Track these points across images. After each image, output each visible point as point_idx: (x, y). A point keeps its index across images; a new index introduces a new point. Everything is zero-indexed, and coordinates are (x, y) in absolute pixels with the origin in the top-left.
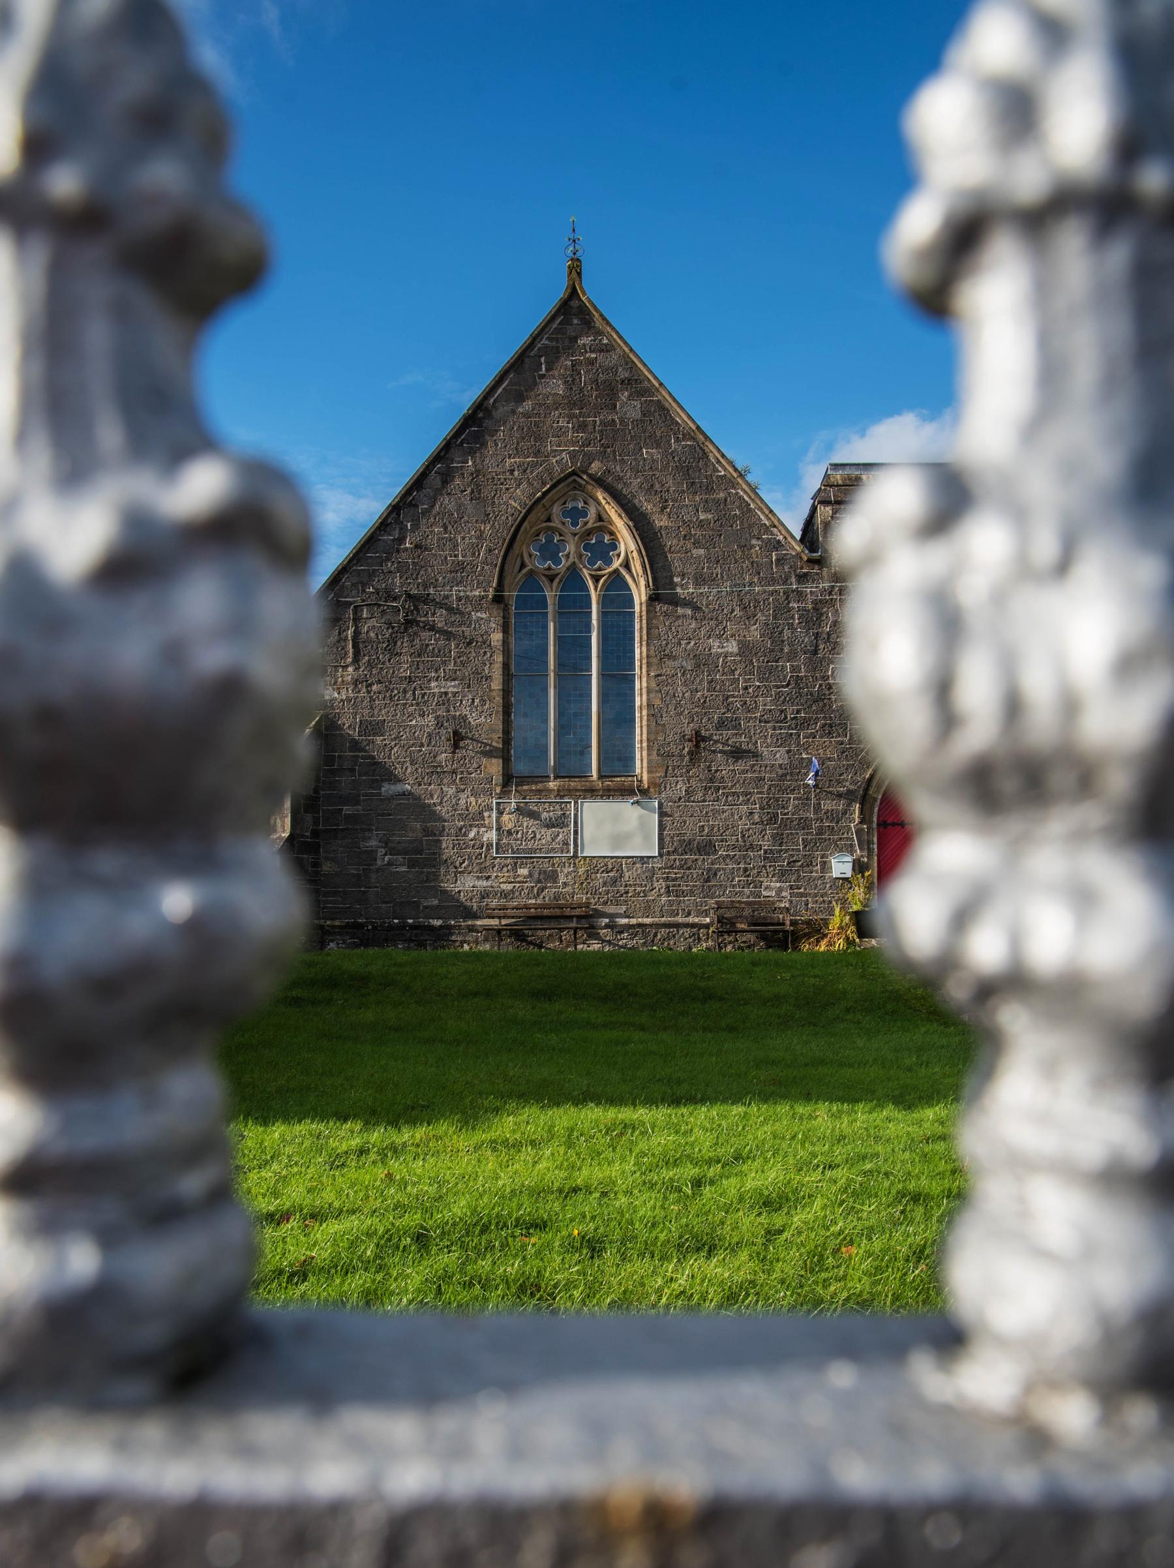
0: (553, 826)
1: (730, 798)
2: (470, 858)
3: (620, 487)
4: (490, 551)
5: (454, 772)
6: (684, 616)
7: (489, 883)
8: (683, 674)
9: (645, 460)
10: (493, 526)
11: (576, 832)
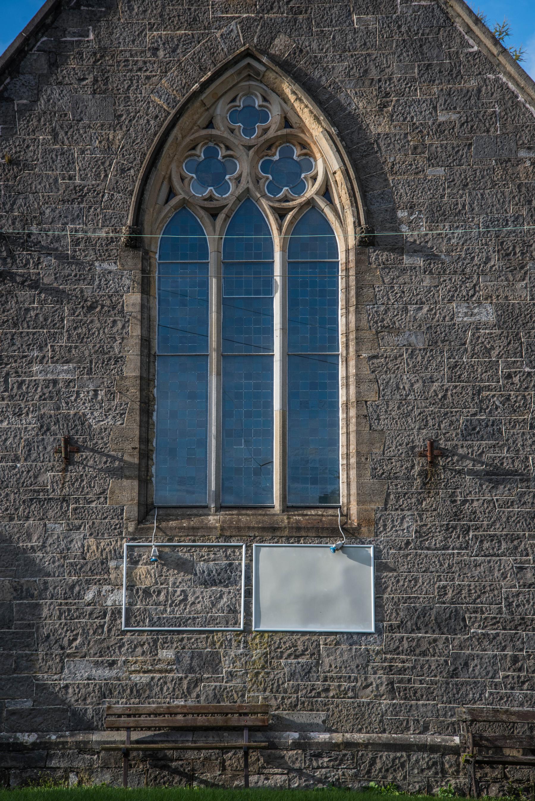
0: (214, 583)
1: (486, 545)
2: (85, 633)
3: (317, 74)
4: (123, 171)
5: (65, 500)
6: (413, 268)
7: (114, 673)
8: (412, 355)
9: (355, 31)
10: (127, 133)
11: (248, 593)
